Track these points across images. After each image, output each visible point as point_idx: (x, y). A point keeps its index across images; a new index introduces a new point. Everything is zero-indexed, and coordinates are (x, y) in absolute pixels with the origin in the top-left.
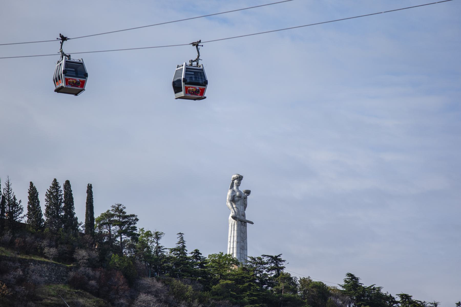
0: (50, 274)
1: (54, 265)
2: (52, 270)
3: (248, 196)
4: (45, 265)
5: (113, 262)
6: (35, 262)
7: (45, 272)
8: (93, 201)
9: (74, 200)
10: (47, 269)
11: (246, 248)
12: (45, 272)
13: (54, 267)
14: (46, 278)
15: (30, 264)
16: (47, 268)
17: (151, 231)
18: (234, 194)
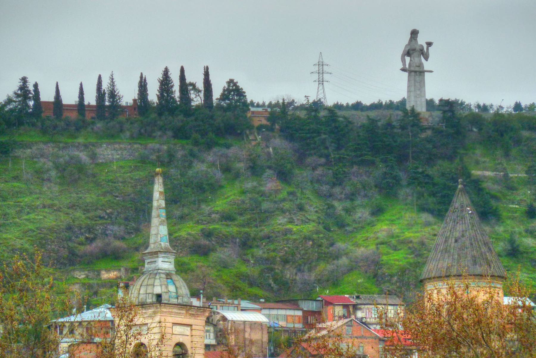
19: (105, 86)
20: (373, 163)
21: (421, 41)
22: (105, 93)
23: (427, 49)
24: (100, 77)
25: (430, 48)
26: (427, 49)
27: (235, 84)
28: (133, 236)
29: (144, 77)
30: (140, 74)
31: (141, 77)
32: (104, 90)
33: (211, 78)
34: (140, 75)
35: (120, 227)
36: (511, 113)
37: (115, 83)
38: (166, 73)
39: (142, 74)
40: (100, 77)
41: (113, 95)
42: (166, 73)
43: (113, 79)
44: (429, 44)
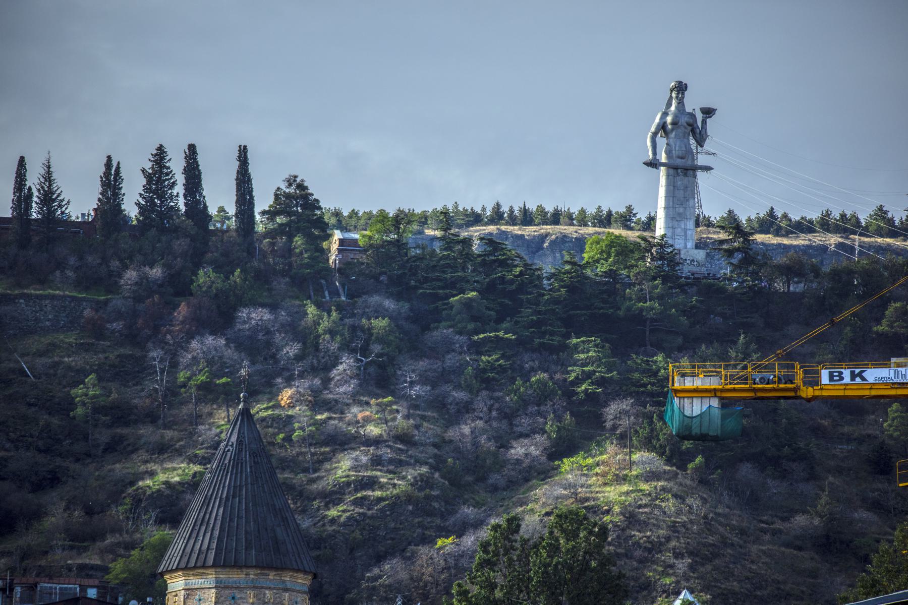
0: (55, 316)
1: (68, 299)
2: (63, 309)
3: (708, 120)
4: (47, 302)
5: (512, 237)
6: (28, 297)
7: (46, 313)
8: (199, 171)
9: (202, 183)
10: (50, 308)
11: (670, 177)
12: (46, 313)
13: (67, 303)
14: (47, 323)
15: (19, 302)
16: (52, 305)
17: (11, 201)
18: (664, 121)
19: (33, 181)
20: (368, 404)
21: (693, 103)
22: (30, 195)
23: (704, 122)
24: (22, 162)
25: (708, 120)
26: (704, 122)
27: (301, 187)
28: (480, 462)
29: (115, 164)
30: (106, 159)
31: (108, 164)
32: (30, 189)
33: (252, 169)
34: (105, 160)
35: (187, 416)
36: (569, 339)
37: (54, 176)
38: (160, 155)
39: (109, 158)
40: (22, 162)
41: (48, 197)
42: (160, 155)
43: (49, 167)
44: (708, 112)
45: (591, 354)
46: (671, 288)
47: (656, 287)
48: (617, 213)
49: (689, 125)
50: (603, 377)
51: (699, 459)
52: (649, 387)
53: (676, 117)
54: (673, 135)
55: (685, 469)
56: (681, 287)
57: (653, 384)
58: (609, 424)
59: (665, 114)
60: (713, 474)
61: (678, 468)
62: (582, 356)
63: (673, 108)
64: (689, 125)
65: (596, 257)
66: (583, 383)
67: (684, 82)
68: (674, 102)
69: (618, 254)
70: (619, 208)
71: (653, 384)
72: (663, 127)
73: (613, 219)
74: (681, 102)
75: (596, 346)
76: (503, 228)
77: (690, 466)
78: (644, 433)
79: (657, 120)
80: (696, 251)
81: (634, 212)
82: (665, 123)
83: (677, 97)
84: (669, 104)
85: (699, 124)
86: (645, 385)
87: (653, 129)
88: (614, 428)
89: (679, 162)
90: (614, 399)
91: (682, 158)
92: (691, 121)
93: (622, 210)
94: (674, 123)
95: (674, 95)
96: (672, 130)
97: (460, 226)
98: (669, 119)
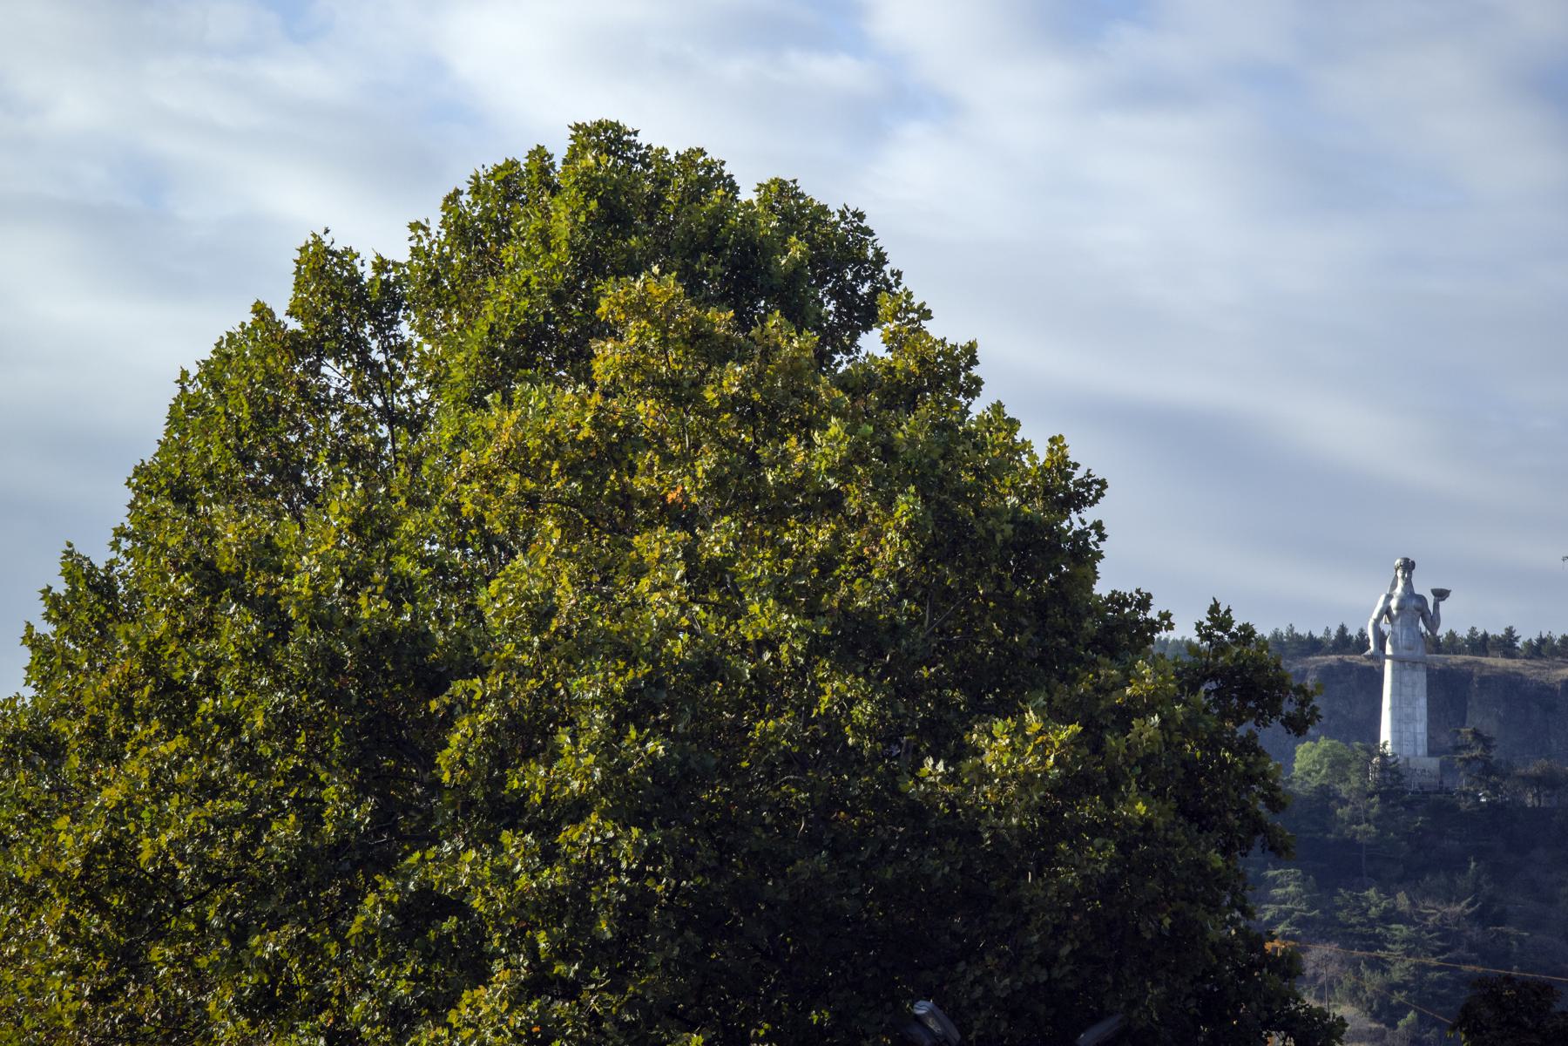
23: (1436, 606)
25: (1441, 603)
26: (1436, 606)
44: (1441, 595)
45: (1291, 889)
46: (1393, 806)
47: (1372, 806)
48: (1494, 637)
49: (1418, 610)
50: (1304, 917)
51: (1411, 1015)
52: (1358, 928)
53: (1402, 601)
54: (1398, 622)
55: (1395, 1027)
56: (1409, 805)
57: (1362, 925)
58: (1309, 973)
59: (1389, 597)
60: (1428, 1032)
61: (1387, 1025)
62: (1280, 891)
63: (1399, 590)
64: (1418, 610)
65: (1308, 768)
66: (1280, 923)
67: (1412, 559)
68: (1400, 584)
69: (1332, 766)
70: (1498, 631)
71: (1362, 925)
72: (1387, 611)
73: (1489, 644)
74: (1408, 583)
75: (1297, 879)
76: (1347, 658)
77: (1401, 1023)
78: (1347, 984)
79: (1380, 605)
80: (1428, 759)
81: (1516, 635)
82: (1389, 607)
83: (1403, 577)
84: (1394, 586)
85: (1431, 607)
86: (1353, 926)
87: (1375, 615)
88: (1315, 977)
89: (1405, 653)
90: (1315, 943)
91: (1410, 649)
92: (1420, 605)
93: (1500, 632)
94: (1399, 608)
95: (1399, 574)
96: (1398, 615)
97: (1292, 657)
98: (1394, 603)
